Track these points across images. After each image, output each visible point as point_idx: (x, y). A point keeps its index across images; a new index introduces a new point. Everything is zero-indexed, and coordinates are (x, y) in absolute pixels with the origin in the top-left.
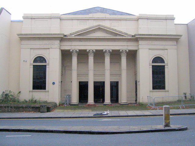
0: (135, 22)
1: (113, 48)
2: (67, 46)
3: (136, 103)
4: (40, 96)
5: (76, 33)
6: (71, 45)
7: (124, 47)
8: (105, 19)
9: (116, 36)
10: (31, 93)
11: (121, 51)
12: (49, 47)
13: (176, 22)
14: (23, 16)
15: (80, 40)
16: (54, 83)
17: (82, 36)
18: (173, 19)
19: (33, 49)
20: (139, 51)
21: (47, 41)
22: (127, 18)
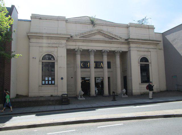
2: (72, 45)
3: (150, 88)
9: (111, 39)
11: (90, 50)
12: (57, 46)
13: (156, 31)
14: (31, 16)
17: (85, 38)
18: (154, 29)
20: (130, 53)
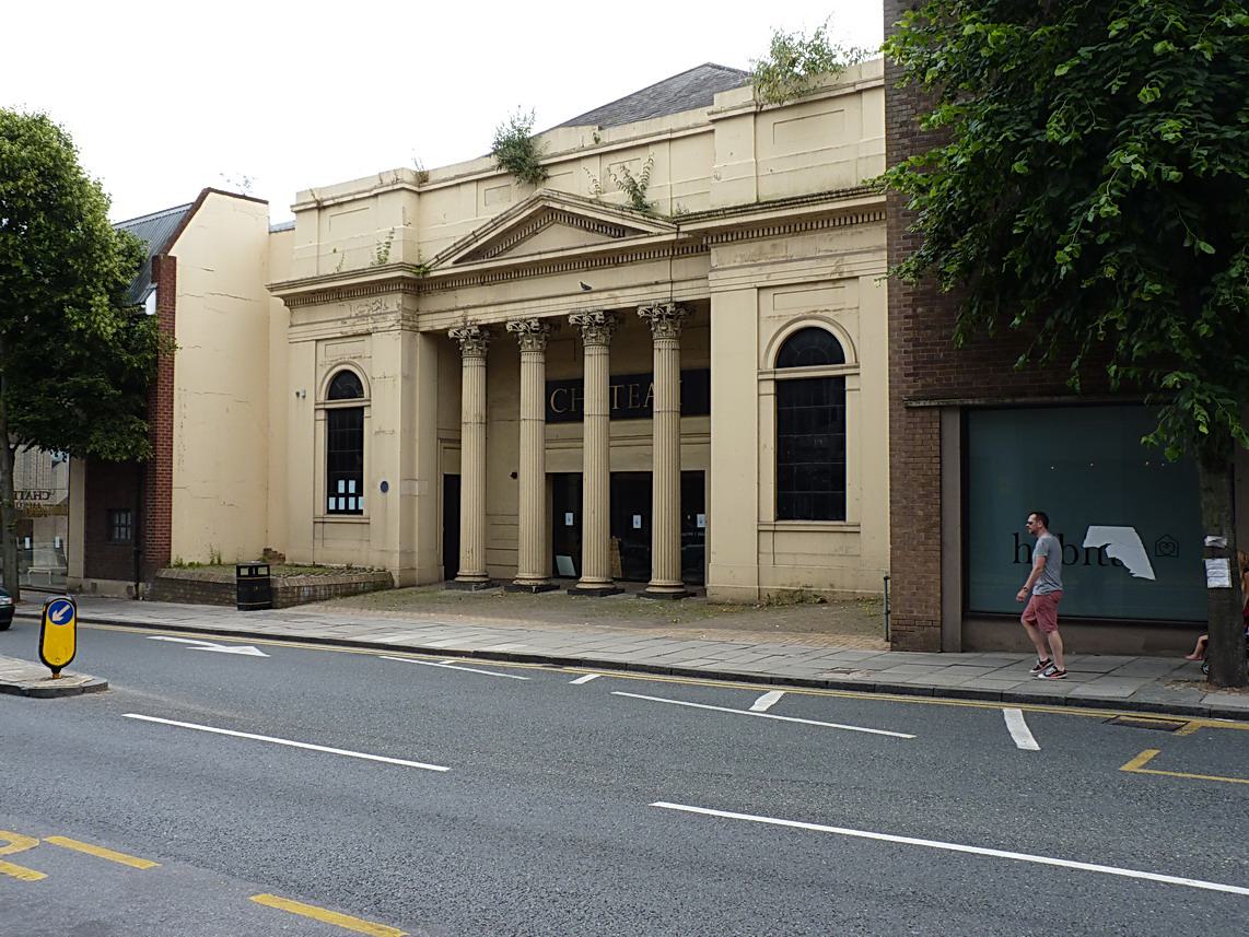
0: (415, 196)
1: (493, 316)
2: (448, 312)
4: (346, 548)
5: (459, 250)
6: (453, 306)
7: (658, 288)
8: (668, 136)
10: (767, 538)
15: (485, 278)
16: (385, 487)
19: (772, 291)
21: (363, 301)
22: (672, 131)
